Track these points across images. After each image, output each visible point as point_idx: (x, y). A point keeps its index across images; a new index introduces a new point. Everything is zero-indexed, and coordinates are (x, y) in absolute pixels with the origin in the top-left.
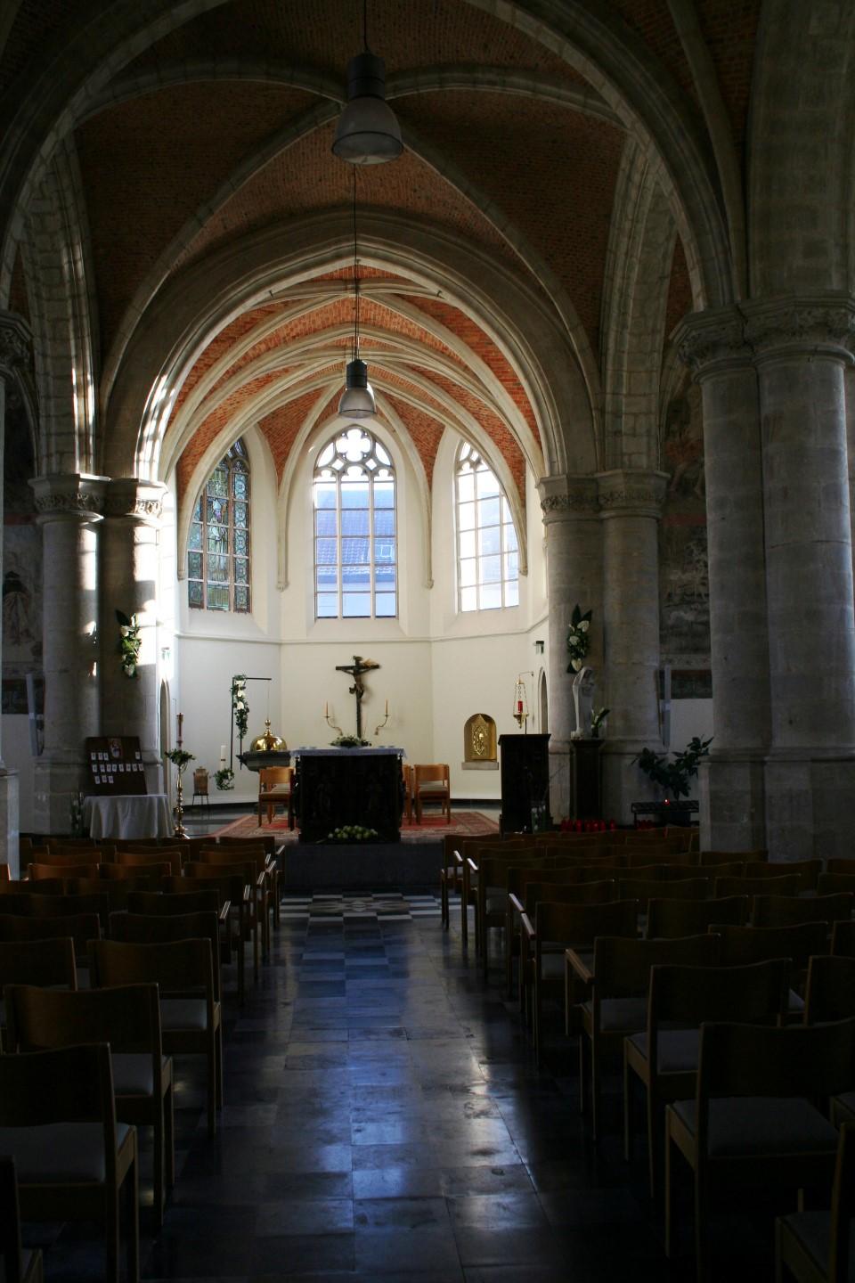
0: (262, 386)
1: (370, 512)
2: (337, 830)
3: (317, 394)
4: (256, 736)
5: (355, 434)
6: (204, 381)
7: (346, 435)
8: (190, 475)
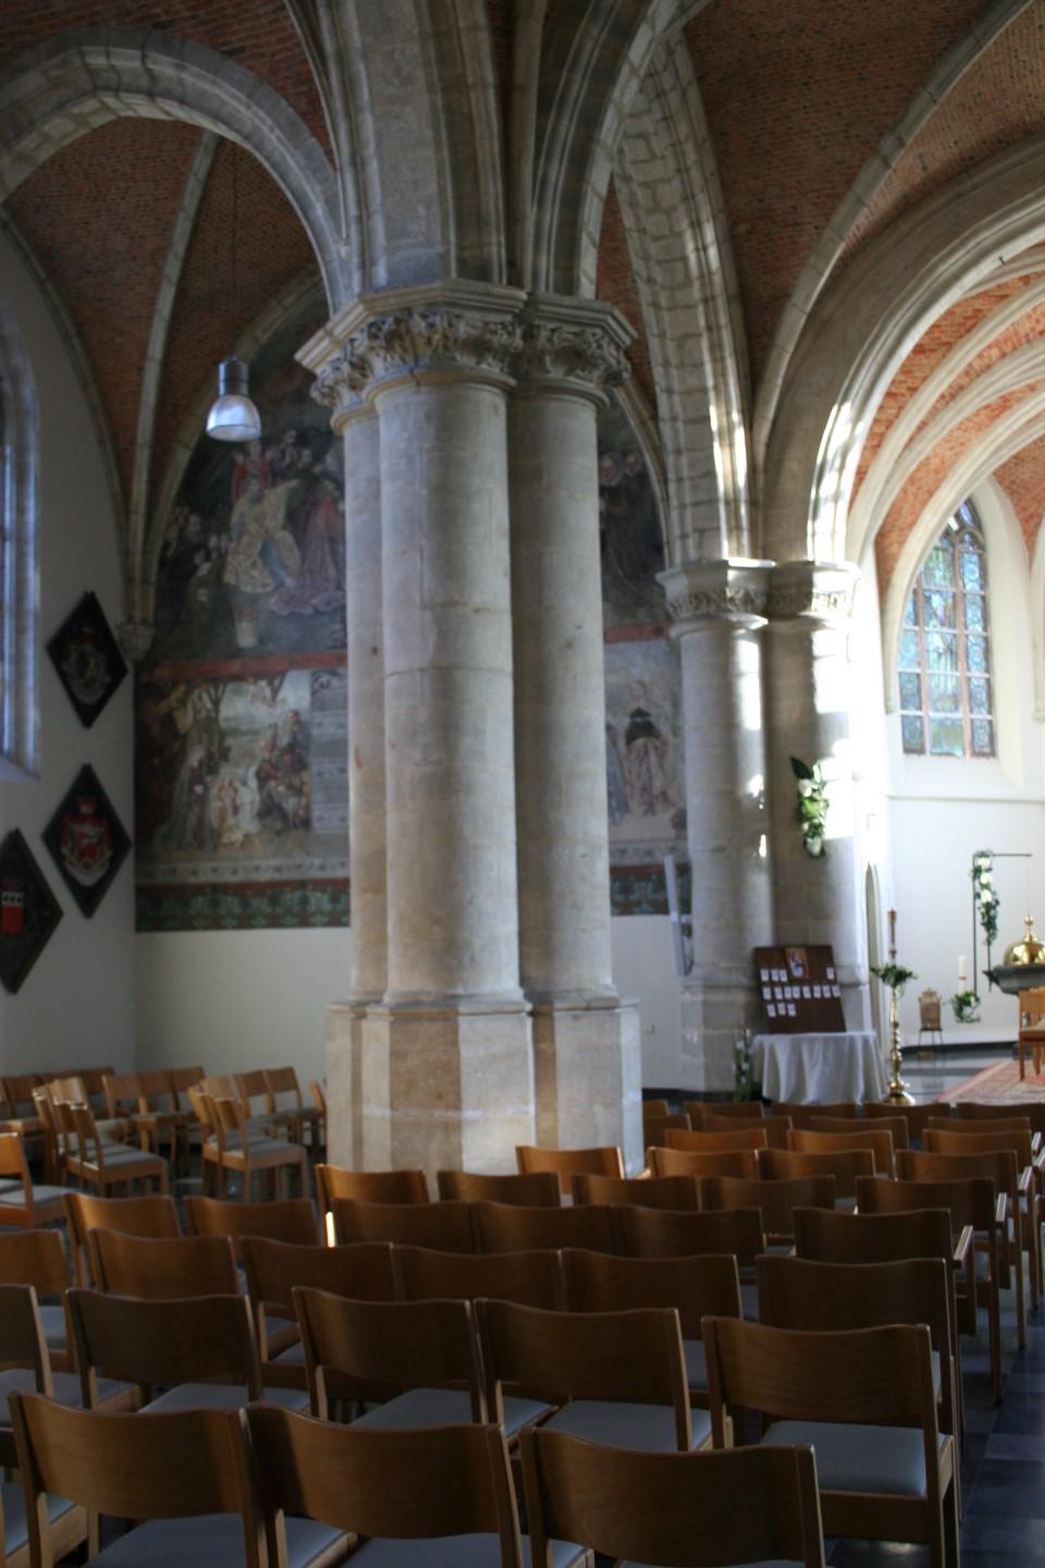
0: (997, 416)
8: (895, 558)
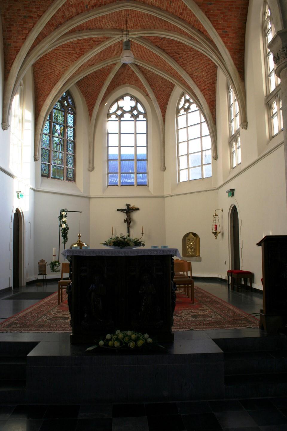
0: (79, 57)
1: (135, 162)
2: (108, 336)
3: (108, 70)
4: (72, 243)
5: (127, 98)
6: (37, 26)
7: (123, 99)
8: (41, 106)
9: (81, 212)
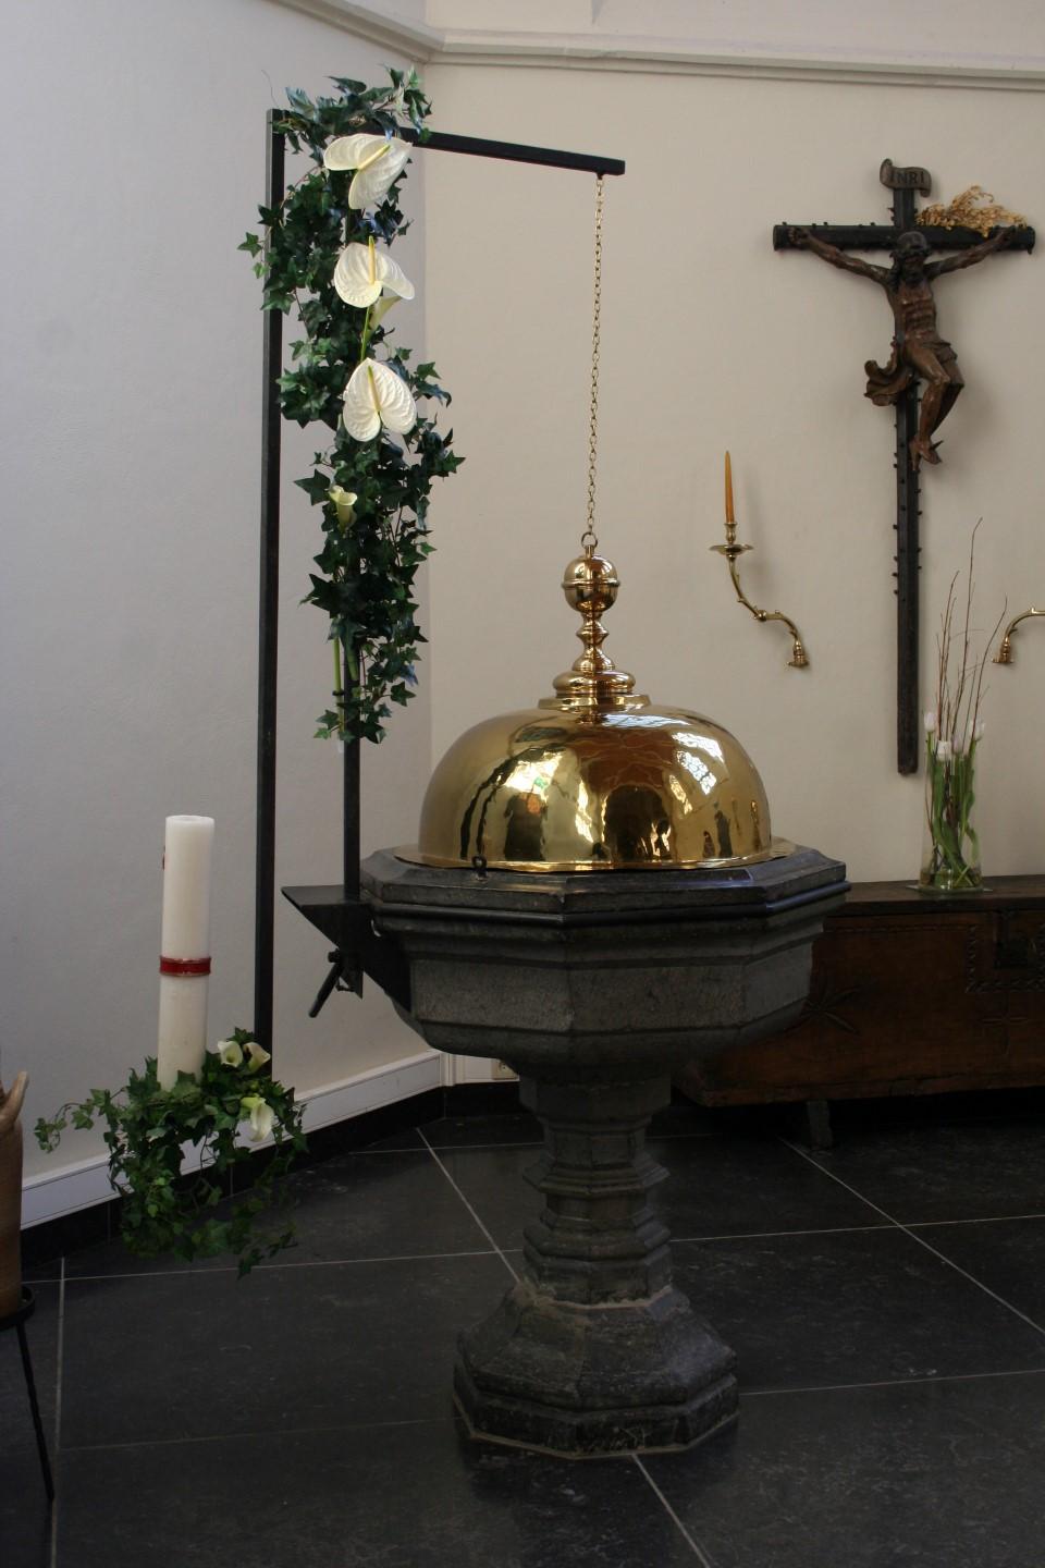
9: (616, 167)
